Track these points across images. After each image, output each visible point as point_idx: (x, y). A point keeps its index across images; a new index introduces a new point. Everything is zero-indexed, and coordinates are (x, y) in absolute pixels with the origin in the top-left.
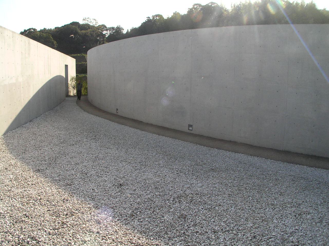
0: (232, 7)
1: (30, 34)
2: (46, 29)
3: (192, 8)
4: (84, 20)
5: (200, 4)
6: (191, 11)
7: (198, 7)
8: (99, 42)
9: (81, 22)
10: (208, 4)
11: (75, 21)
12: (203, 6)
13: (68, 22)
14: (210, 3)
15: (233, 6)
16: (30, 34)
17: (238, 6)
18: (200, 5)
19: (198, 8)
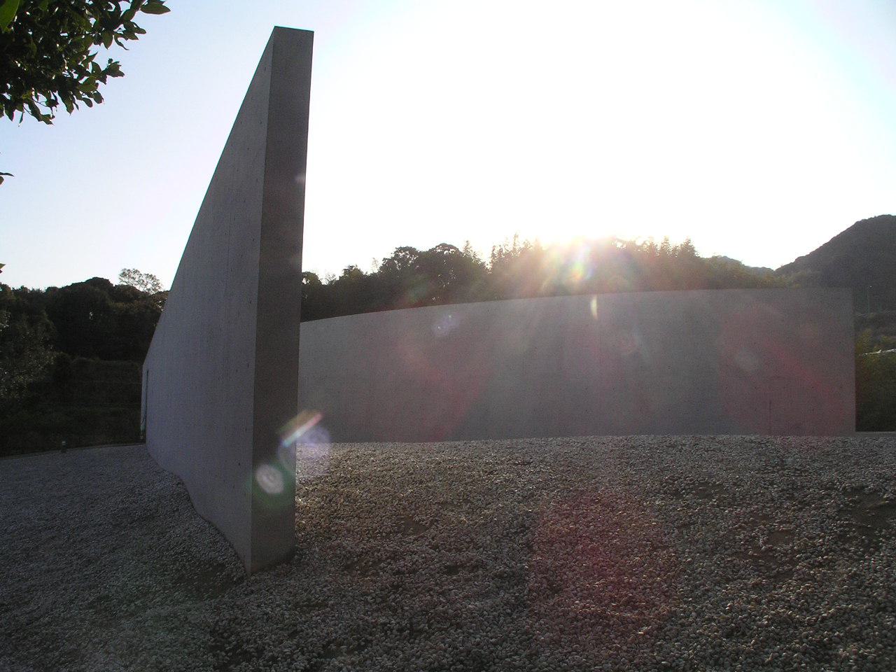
0: (493, 255)
1: (288, 57)
2: (26, 288)
3: (393, 259)
4: (124, 274)
5: (415, 249)
6: (388, 265)
7: (408, 256)
8: (339, 647)
9: (115, 281)
10: (433, 249)
11: (100, 276)
12: (421, 254)
13: (82, 278)
14: (438, 246)
15: (497, 249)
16: (288, 57)
17: (508, 255)
18: (412, 251)
19: (409, 259)
